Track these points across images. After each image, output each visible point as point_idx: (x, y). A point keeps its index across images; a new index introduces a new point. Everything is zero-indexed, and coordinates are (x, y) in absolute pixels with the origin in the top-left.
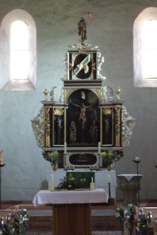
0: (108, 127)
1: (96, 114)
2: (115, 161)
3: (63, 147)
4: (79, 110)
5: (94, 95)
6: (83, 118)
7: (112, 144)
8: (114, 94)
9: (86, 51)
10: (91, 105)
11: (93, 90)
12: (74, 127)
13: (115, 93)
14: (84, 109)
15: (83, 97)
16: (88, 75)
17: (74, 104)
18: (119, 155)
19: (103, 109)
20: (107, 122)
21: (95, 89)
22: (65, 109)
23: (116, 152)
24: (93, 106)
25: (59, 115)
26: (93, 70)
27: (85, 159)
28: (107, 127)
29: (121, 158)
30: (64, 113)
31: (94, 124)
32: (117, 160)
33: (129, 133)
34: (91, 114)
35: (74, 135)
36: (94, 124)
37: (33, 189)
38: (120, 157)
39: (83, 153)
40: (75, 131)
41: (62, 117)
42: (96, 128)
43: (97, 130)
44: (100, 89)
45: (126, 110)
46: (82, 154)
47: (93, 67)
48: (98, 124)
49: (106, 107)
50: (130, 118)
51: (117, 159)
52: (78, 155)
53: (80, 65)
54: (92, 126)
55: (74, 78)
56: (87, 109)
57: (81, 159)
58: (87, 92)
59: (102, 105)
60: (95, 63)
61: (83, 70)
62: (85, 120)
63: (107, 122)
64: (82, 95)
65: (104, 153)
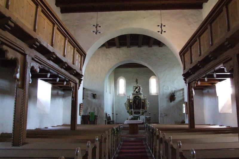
15: (137, 98)
16: (138, 92)
41: (132, 102)
62: (137, 103)
63: (143, 104)
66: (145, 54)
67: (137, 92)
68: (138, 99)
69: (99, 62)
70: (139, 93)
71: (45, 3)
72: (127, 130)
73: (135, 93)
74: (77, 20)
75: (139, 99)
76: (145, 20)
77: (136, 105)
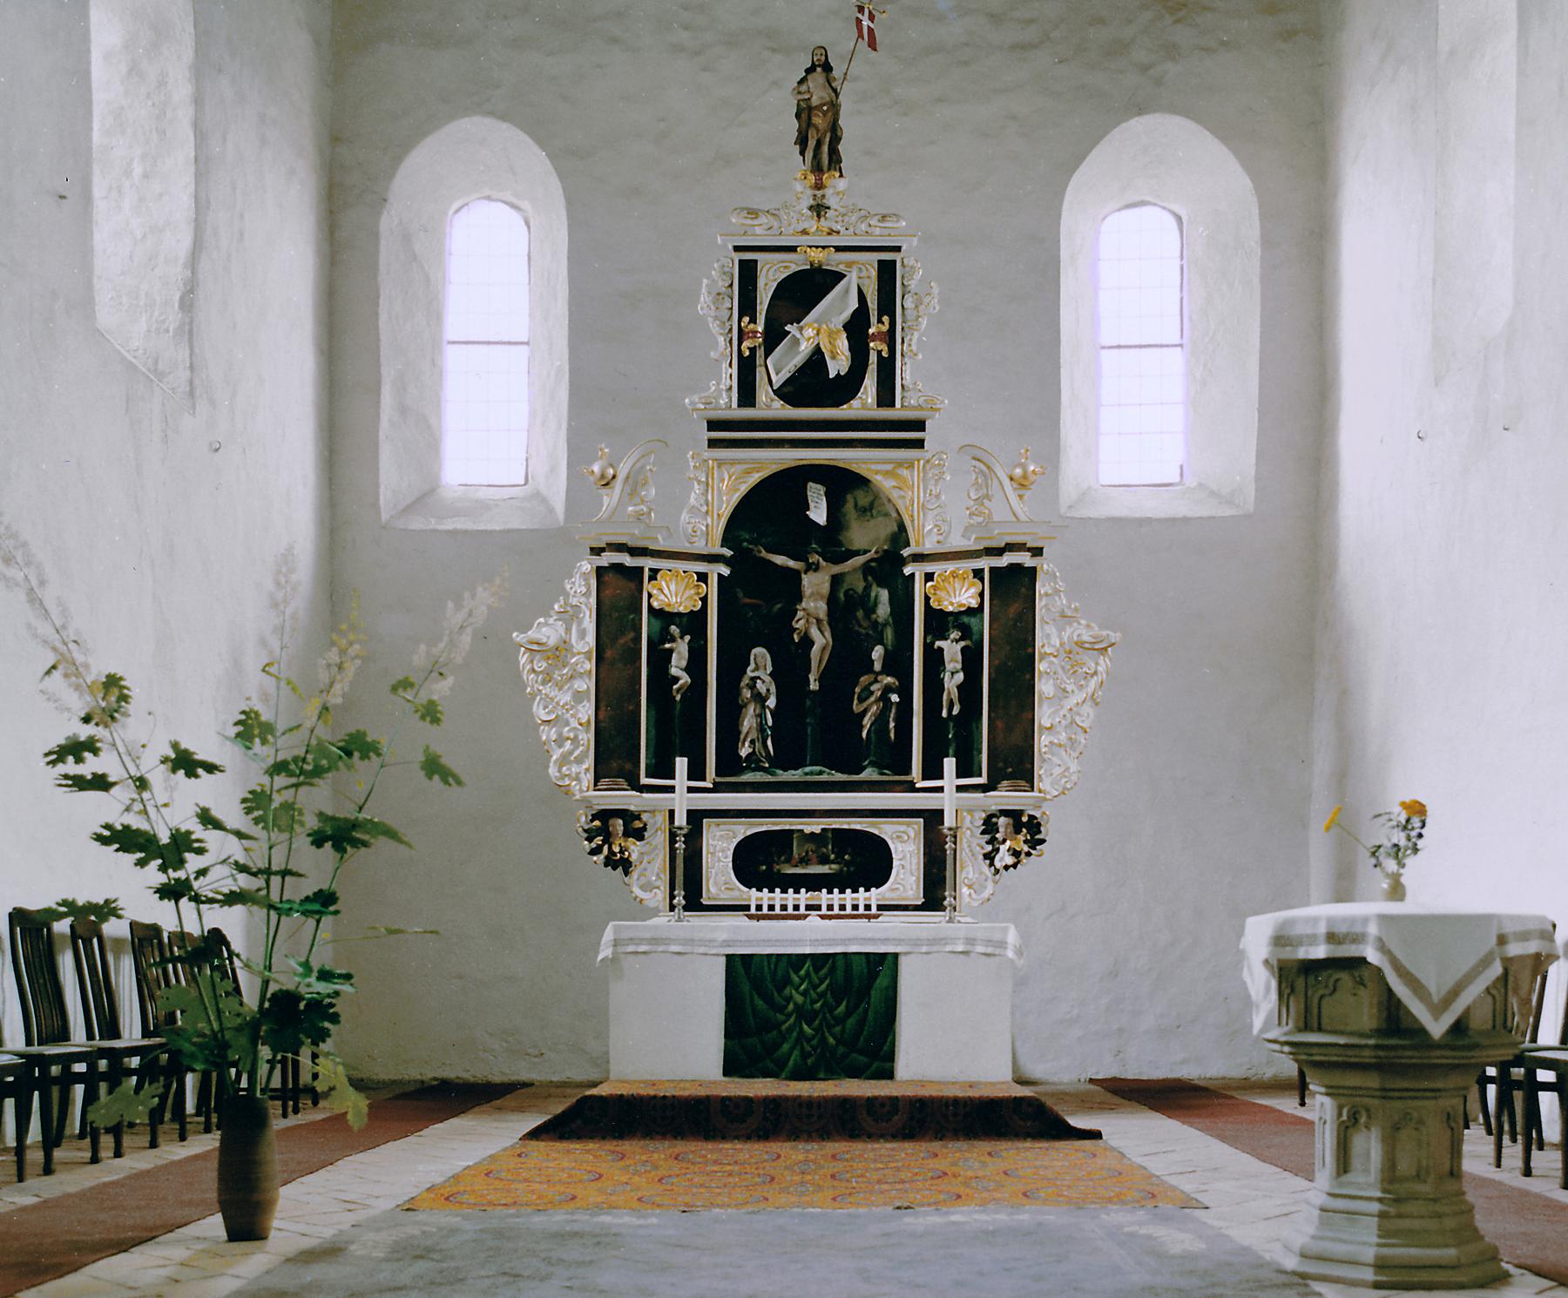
0: (960, 677)
1: (883, 610)
2: (997, 871)
3: (940, 789)
4: (790, 587)
5: (873, 506)
6: (814, 633)
7: (980, 776)
8: (994, 489)
9: (838, 249)
10: (860, 560)
11: (876, 478)
12: (768, 679)
13: (1007, 482)
14: (815, 585)
15: (818, 513)
16: (847, 387)
17: (764, 554)
18: (1021, 837)
19: (929, 577)
20: (951, 649)
21: (889, 467)
22: (713, 581)
23: (1002, 821)
24: (866, 569)
25: (682, 609)
26: (873, 357)
27: (824, 860)
28: (952, 681)
29: (1028, 854)
30: (704, 600)
31: (877, 667)
32: (1006, 868)
33: (1079, 714)
34: (860, 614)
35: (761, 728)
36: (877, 667)
37: (146, 1268)
38: (1026, 848)
39: (814, 826)
40: (772, 702)
41: (694, 623)
42: (888, 689)
43: (895, 698)
44: (910, 466)
45: (1061, 585)
46: (807, 830)
47: (874, 337)
48: (898, 663)
49: (950, 567)
50: (1082, 631)
51: (1010, 860)
52: (789, 834)
53: (801, 329)
54: (864, 679)
55: (769, 405)
56: (836, 580)
57: (804, 861)
58: (842, 483)
59: (919, 558)
60: (886, 319)
61: (817, 360)
62: (821, 641)
63: (951, 649)
64: (812, 505)
65: (572, 592)
68: (831, 542)
70: (864, 403)
75: (865, 537)
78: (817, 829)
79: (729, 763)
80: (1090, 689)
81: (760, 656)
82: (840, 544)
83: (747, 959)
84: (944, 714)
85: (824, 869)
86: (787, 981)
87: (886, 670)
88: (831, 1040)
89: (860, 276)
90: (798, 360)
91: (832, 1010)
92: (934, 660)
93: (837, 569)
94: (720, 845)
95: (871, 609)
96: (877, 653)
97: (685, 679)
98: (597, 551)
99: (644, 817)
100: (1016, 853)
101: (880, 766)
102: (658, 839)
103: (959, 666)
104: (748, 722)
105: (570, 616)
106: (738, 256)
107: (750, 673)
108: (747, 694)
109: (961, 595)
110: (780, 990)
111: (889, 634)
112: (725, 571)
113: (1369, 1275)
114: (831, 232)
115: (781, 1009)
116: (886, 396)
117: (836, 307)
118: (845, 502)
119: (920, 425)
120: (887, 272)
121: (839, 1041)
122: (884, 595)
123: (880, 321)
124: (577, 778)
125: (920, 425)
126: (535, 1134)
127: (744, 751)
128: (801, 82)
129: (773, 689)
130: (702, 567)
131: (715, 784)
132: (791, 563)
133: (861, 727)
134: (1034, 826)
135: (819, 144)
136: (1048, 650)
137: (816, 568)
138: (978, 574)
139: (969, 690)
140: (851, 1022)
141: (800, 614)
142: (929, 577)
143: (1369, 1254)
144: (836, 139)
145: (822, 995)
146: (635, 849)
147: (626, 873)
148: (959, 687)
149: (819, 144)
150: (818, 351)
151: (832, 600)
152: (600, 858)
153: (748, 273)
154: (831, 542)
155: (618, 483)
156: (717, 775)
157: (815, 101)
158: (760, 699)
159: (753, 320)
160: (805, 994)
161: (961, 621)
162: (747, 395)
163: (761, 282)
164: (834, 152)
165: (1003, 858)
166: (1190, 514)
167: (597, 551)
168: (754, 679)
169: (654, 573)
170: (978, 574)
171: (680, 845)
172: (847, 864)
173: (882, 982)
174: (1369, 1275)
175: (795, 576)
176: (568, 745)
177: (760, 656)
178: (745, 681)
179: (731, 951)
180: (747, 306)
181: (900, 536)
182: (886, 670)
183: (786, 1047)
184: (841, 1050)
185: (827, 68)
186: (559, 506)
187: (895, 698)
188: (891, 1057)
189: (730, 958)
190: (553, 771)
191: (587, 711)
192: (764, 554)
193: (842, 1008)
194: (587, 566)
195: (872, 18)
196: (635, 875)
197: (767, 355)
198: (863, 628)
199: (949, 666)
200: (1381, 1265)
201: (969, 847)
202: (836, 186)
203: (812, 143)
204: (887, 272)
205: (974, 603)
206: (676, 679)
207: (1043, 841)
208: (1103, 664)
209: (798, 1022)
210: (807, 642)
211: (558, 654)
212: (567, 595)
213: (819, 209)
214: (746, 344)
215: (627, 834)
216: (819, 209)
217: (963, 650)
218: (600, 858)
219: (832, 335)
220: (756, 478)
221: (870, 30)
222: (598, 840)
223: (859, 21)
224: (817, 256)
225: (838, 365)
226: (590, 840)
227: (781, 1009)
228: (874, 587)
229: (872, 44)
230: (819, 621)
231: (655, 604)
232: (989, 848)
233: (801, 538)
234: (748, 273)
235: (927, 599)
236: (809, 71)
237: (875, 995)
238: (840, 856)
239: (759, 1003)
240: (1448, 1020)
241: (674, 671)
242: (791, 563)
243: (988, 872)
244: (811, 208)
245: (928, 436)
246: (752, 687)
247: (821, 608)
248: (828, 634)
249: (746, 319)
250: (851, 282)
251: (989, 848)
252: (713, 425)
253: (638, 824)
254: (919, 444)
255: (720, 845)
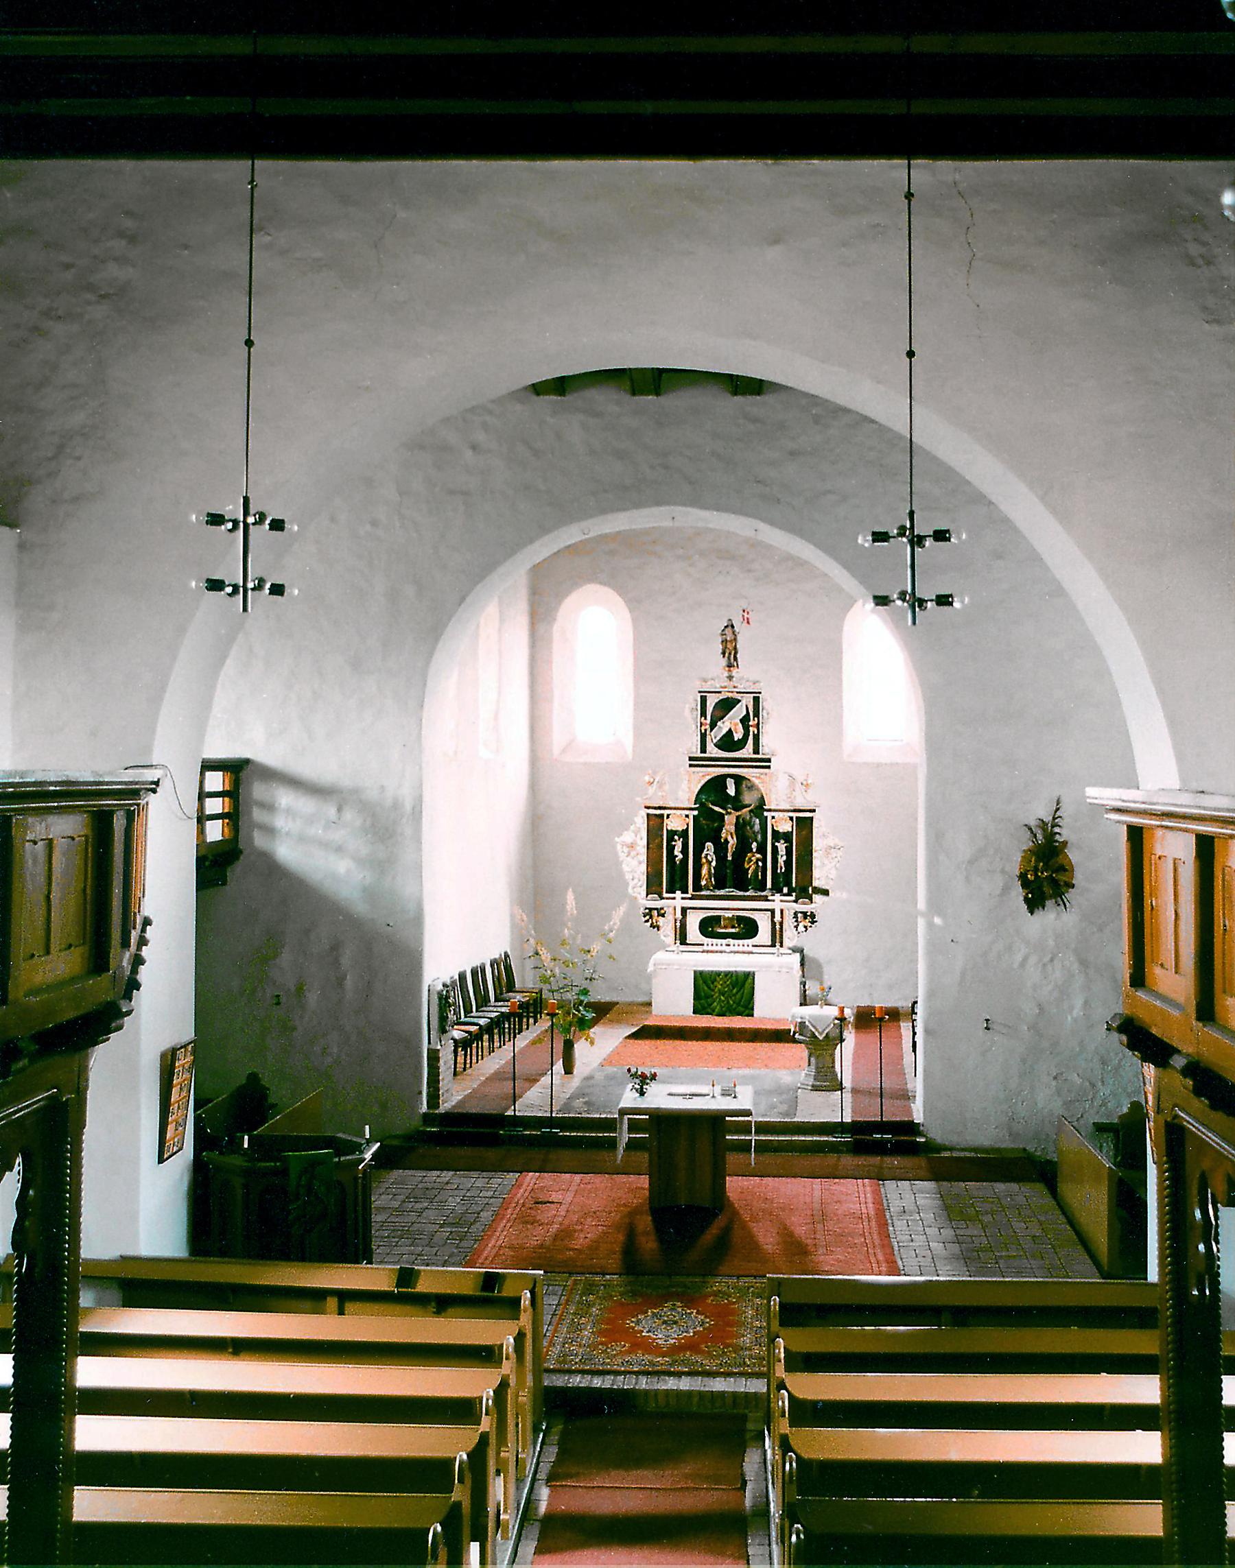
0: (784, 858)
1: (757, 828)
5: (751, 787)
6: (729, 838)
9: (737, 692)
10: (748, 809)
14: (730, 820)
15: (731, 791)
16: (741, 744)
17: (711, 806)
18: (807, 921)
19: (773, 817)
20: (782, 847)
26: (751, 733)
27: (733, 927)
28: (781, 860)
30: (688, 825)
31: (754, 850)
36: (754, 850)
38: (810, 924)
39: (729, 914)
40: (714, 864)
41: (684, 834)
42: (758, 860)
43: (760, 864)
46: (727, 915)
48: (762, 849)
49: (781, 814)
52: (719, 917)
55: (713, 751)
57: (725, 927)
59: (770, 810)
60: (756, 719)
62: (732, 842)
63: (782, 847)
66: (792, 453)
67: (728, 743)
68: (737, 803)
69: (374, 523)
70: (747, 751)
71: (1142, 869)
72: (377, 1209)
73: (713, 751)
74: (121, 234)
75: (749, 798)
76: (773, 253)
77: (721, 848)
78: (730, 916)
79: (697, 887)
80: (834, 864)
81: (709, 845)
82: (740, 802)
83: (701, 973)
84: (779, 871)
85: (733, 930)
86: (715, 980)
87: (758, 852)
88: (731, 1002)
89: (747, 701)
90: (724, 731)
91: (732, 991)
92: (775, 850)
93: (739, 813)
94: (693, 921)
95: (752, 827)
96: (754, 845)
97: (681, 856)
98: (648, 808)
99: (665, 909)
100: (805, 927)
101: (756, 889)
102: (670, 917)
103: (784, 853)
104: (704, 871)
105: (636, 833)
106: (699, 695)
107: (705, 852)
108: (704, 860)
109: (785, 827)
110: (713, 983)
111: (759, 837)
112: (696, 813)
113: (810, 1088)
114: (735, 687)
115: (713, 990)
116: (756, 751)
117: (738, 712)
118: (742, 784)
119: (769, 760)
120: (756, 700)
121: (734, 1003)
122: (758, 821)
123: (754, 720)
124: (640, 894)
125: (769, 760)
126: (629, 1037)
127: (703, 883)
128: (723, 630)
129: (714, 858)
130: (687, 812)
131: (692, 895)
132: (721, 811)
133: (748, 874)
134: (813, 916)
135: (730, 654)
136: (817, 848)
137: (730, 813)
138: (791, 818)
139: (788, 863)
140: (738, 996)
141: (724, 831)
142: (773, 817)
143: (811, 1083)
144: (736, 653)
145: (728, 985)
146: (661, 921)
147: (658, 930)
148: (784, 861)
149: (730, 654)
150: (730, 730)
151: (737, 825)
152: (649, 924)
153: (704, 700)
154: (737, 803)
155: (655, 783)
156: (693, 891)
157: (728, 639)
158: (709, 863)
159: (706, 719)
160: (721, 985)
161: (787, 837)
162: (703, 750)
163: (708, 704)
164: (735, 659)
165: (801, 928)
166: (899, 761)
167: (648, 808)
168: (707, 855)
169: (668, 816)
170: (791, 818)
171: (678, 924)
172: (743, 928)
173: (750, 981)
174: (810, 1088)
175: (723, 815)
176: (636, 881)
177: (709, 845)
178: (703, 855)
179: (695, 969)
180: (703, 714)
181: (762, 801)
182: (758, 852)
183: (715, 1004)
184: (735, 1006)
185: (733, 626)
186: (629, 750)
187: (760, 864)
188: (752, 1009)
189: (695, 972)
190: (630, 890)
191: (644, 867)
192: (711, 806)
193: (735, 991)
194: (644, 812)
195: (748, 613)
196: (662, 930)
197: (711, 731)
198: (750, 834)
199: (780, 853)
200: (813, 1086)
201: (789, 922)
202: (734, 672)
203: (727, 655)
204: (756, 700)
205: (790, 830)
206: (677, 856)
207: (816, 921)
208: (840, 853)
209: (719, 996)
210: (727, 841)
211: (632, 846)
212: (635, 823)
213: (730, 678)
214: (703, 728)
215: (658, 916)
216: (730, 678)
217: (786, 847)
218: (649, 924)
219: (736, 725)
220: (708, 778)
221: (748, 619)
222: (648, 917)
223: (743, 616)
224: (730, 695)
225: (738, 736)
226: (645, 916)
227: (713, 990)
228: (754, 818)
229: (748, 623)
230: (731, 834)
231: (669, 828)
232: (796, 924)
233: (724, 800)
234: (704, 700)
235: (773, 825)
236: (726, 627)
237: (747, 985)
238: (739, 925)
239: (706, 988)
240: (824, 1035)
241: (676, 853)
242: (721, 811)
243: (796, 933)
244: (727, 677)
245: (771, 764)
246: (706, 857)
247: (732, 828)
248: (735, 839)
249: (703, 718)
250: (744, 702)
251: (796, 924)
252: (691, 759)
253: (662, 912)
254: (769, 767)
255: (693, 921)
